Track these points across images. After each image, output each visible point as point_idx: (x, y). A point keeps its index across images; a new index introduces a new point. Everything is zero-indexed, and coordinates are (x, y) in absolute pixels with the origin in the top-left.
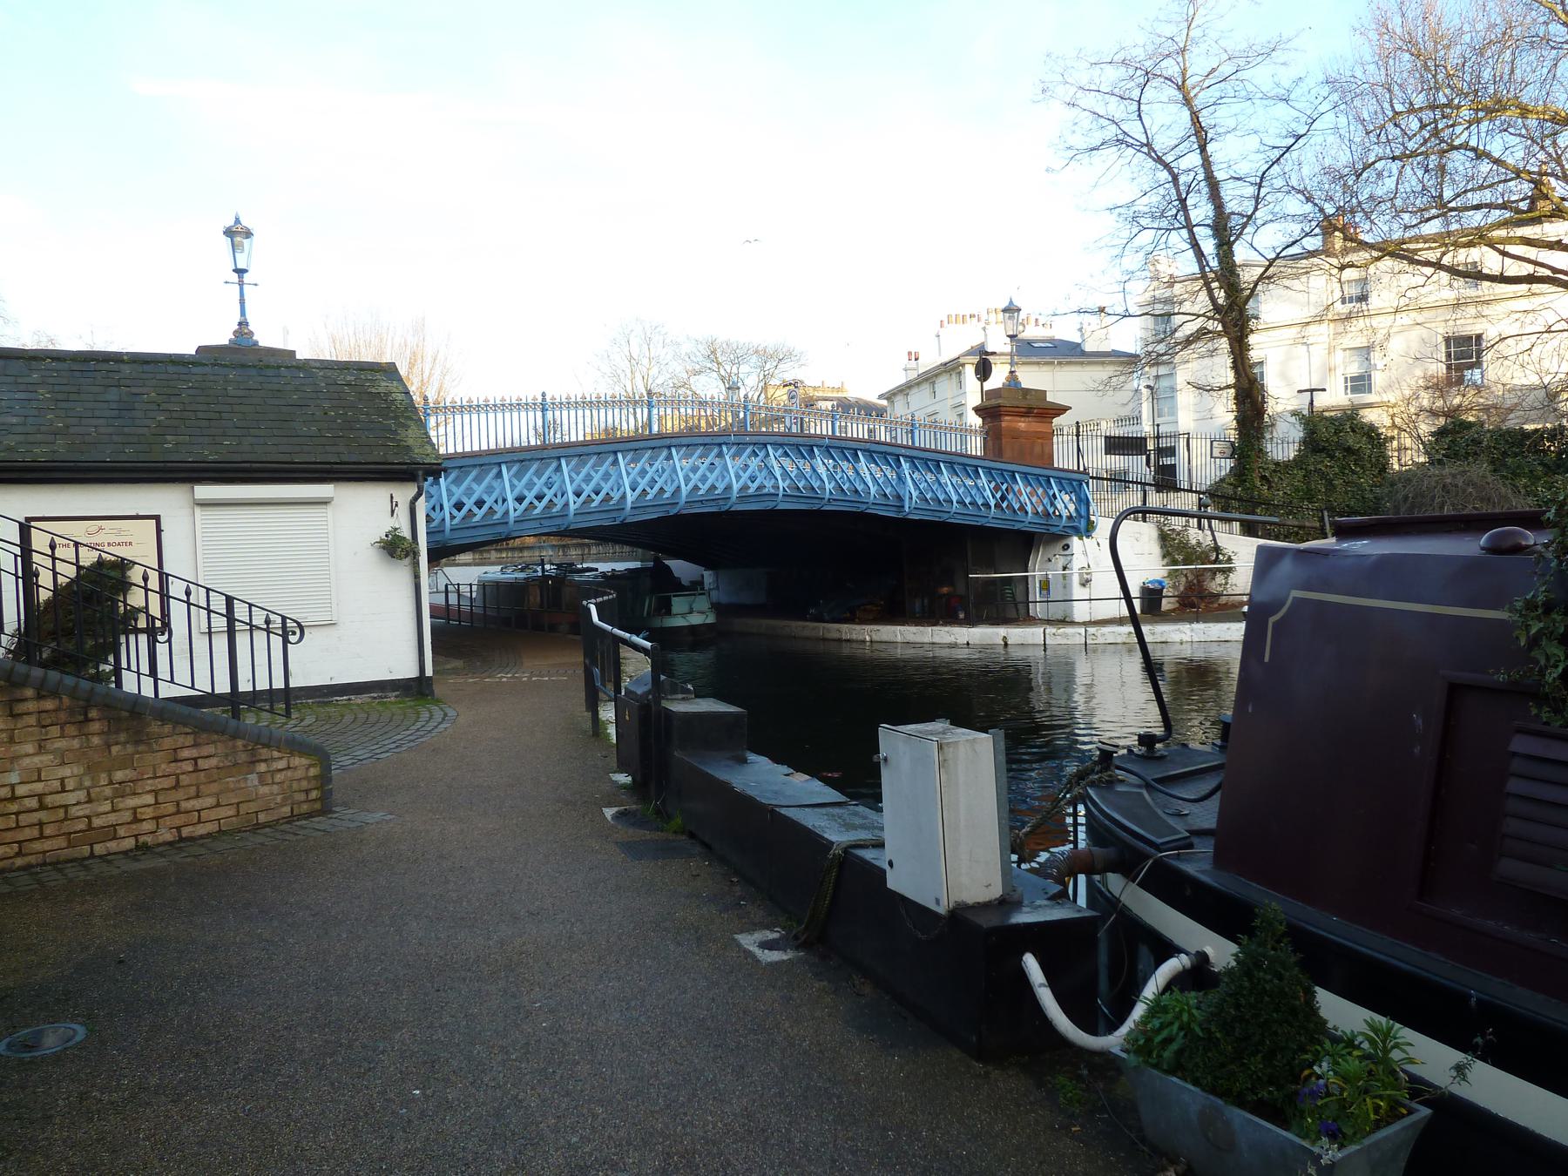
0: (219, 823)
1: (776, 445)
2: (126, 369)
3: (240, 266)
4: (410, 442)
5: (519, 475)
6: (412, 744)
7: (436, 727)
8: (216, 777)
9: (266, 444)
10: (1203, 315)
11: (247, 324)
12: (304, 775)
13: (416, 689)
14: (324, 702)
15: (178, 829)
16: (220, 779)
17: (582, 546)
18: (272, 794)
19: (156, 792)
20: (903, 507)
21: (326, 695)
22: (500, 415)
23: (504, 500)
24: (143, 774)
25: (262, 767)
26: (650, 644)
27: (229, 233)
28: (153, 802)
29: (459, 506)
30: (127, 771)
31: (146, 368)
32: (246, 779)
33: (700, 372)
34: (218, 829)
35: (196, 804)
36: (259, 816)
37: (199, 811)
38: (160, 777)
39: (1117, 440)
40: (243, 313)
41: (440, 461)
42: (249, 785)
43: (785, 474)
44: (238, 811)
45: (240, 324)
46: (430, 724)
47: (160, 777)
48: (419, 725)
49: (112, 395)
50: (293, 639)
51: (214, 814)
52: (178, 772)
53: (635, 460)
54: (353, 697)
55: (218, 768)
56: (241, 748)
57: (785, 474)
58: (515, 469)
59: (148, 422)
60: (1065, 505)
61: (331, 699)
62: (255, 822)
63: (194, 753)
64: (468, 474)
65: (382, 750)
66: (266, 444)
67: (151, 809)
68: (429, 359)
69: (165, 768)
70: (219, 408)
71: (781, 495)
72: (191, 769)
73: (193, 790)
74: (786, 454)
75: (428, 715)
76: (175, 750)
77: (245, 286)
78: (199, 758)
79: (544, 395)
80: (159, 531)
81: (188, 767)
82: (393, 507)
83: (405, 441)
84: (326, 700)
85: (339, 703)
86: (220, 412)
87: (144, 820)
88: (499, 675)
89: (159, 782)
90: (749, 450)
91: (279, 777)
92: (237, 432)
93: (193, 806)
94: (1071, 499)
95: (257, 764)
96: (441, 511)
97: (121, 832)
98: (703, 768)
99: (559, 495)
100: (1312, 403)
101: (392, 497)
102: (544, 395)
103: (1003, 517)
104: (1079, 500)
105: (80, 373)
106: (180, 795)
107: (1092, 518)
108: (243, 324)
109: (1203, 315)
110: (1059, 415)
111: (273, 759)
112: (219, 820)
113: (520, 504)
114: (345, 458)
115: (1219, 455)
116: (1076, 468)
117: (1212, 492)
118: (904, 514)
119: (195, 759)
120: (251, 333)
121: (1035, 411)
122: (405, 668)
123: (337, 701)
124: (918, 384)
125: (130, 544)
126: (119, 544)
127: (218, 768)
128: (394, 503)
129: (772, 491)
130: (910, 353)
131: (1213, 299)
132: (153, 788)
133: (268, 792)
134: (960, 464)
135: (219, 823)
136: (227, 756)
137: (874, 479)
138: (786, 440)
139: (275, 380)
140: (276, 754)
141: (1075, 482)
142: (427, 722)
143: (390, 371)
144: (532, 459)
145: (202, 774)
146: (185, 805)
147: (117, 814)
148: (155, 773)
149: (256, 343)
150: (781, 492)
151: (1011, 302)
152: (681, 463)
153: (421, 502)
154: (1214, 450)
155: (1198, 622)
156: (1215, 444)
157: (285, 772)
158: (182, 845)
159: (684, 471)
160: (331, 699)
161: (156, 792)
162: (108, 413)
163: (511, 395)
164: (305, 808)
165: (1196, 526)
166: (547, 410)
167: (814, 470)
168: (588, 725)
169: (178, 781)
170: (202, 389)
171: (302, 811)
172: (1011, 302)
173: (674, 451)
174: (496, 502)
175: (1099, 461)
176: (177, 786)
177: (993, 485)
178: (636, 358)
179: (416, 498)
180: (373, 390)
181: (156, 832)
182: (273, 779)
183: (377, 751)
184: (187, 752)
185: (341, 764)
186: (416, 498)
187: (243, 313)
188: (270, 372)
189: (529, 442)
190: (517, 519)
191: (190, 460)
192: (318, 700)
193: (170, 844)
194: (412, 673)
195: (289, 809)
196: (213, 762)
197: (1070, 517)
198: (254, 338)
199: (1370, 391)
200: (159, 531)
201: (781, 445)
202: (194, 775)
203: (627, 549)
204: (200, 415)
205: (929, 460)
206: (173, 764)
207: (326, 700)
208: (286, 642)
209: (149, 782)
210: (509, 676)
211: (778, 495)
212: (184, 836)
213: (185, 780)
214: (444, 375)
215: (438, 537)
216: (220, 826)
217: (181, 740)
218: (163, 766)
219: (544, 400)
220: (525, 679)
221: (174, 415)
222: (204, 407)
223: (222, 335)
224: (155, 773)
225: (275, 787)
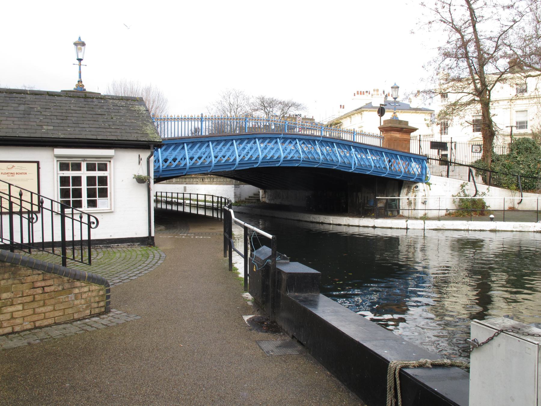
0: (55, 319)
1: (300, 140)
2: (29, 97)
3: (80, 57)
4: (148, 132)
5: (192, 148)
6: (146, 272)
7: (157, 262)
8: (53, 296)
9: (86, 131)
10: (472, 93)
11: (81, 82)
12: (96, 295)
13: (147, 241)
14: (107, 246)
15: (34, 322)
16: (56, 297)
17: (210, 178)
18: (81, 304)
19: (23, 304)
20: (351, 167)
21: (108, 243)
22: (190, 123)
23: (185, 159)
24: (17, 295)
25: (76, 291)
26: (272, 236)
27: (76, 44)
28: (21, 309)
29: (166, 161)
30: (8, 294)
31: (37, 97)
32: (68, 297)
33: (257, 110)
34: (54, 322)
35: (43, 309)
36: (75, 315)
37: (44, 313)
38: (25, 296)
39: (439, 144)
40: (80, 77)
41: (161, 141)
42: (70, 300)
43: (303, 152)
44: (64, 313)
45: (79, 82)
46: (154, 261)
47: (25, 296)
48: (149, 260)
49: (22, 107)
50: (93, 226)
51: (52, 315)
52: (34, 293)
53: (240, 143)
54: (120, 245)
55: (54, 292)
56: (66, 281)
57: (303, 152)
58: (190, 146)
59: (36, 120)
60: (415, 168)
61: (110, 245)
62: (72, 318)
63: (43, 284)
64: (171, 146)
65: (133, 275)
66: (86, 131)
67: (20, 312)
69: (27, 292)
70: (67, 115)
71: (301, 160)
72: (41, 292)
73: (42, 303)
74: (304, 143)
75: (152, 256)
76: (33, 282)
77: (81, 66)
78: (45, 286)
79: (202, 115)
80: (38, 168)
81: (40, 291)
82: (140, 160)
83: (146, 131)
84: (108, 245)
85: (114, 247)
86: (67, 117)
87: (17, 318)
88: (181, 235)
89: (25, 299)
90: (288, 141)
91: (84, 296)
92: (74, 125)
93: (42, 310)
94: (419, 167)
95: (74, 289)
96: (158, 162)
97: (5, 324)
98: (306, 307)
99: (208, 157)
100: (512, 131)
101: (139, 156)
102: (202, 115)
103: (392, 173)
104: (422, 168)
105: (9, 98)
106: (35, 305)
107: (428, 175)
108: (80, 81)
109: (472, 93)
110: (413, 132)
111: (82, 287)
112: (54, 317)
113: (192, 160)
114: (120, 138)
115: (475, 151)
116: (418, 154)
118: (352, 170)
119: (43, 287)
120: (83, 86)
121: (404, 130)
122: (144, 233)
123: (113, 246)
125: (26, 173)
126: (21, 174)
127: (54, 292)
128: (140, 159)
129: (298, 159)
131: (475, 86)
132: (22, 302)
133: (79, 303)
134: (374, 150)
135: (55, 319)
136: (59, 285)
137: (340, 156)
138: (304, 137)
139: (91, 103)
140: (83, 284)
141: (422, 159)
142: (153, 259)
143: (140, 101)
144: (197, 141)
145: (47, 294)
146: (38, 310)
147: (3, 315)
148: (23, 294)
149: (85, 90)
150: (302, 160)
151: (395, 84)
152: (259, 145)
153: (152, 159)
154: (473, 149)
155: (471, 221)
156: (474, 147)
157: (87, 293)
158: (36, 331)
159: (261, 148)
160: (110, 245)
161: (23, 304)
162: (19, 116)
163: (189, 114)
164: (97, 311)
165: (468, 180)
166: (203, 121)
167: (315, 150)
168: (227, 264)
169: (34, 298)
170: (60, 106)
171: (96, 312)
172: (395, 84)
173: (257, 140)
174: (181, 159)
175: (427, 150)
176: (34, 301)
177: (388, 159)
178: (232, 104)
179: (150, 157)
180: (133, 109)
181: (22, 324)
182: (81, 297)
183: (131, 275)
184: (39, 283)
185: (114, 282)
186: (150, 157)
187: (80, 77)
188: (90, 100)
189: (188, 135)
190: (190, 167)
191: (53, 137)
192: (104, 245)
193: (30, 330)
194: (146, 235)
195: (89, 311)
196: (52, 288)
197: (419, 175)
198: (84, 88)
199: (526, 128)
200: (38, 168)
201: (302, 139)
202: (43, 295)
203: (228, 180)
204: (59, 117)
205: (362, 148)
206: (32, 290)
207: (108, 245)
208: (90, 227)
209: (20, 299)
210: (185, 235)
211: (300, 160)
212: (37, 326)
213: (38, 297)
214: (157, 108)
215: (158, 174)
216: (55, 321)
217: (36, 277)
218: (27, 291)
219: (202, 117)
220: (192, 237)
222: (60, 114)
223: (71, 86)
224: (23, 294)
225: (83, 300)
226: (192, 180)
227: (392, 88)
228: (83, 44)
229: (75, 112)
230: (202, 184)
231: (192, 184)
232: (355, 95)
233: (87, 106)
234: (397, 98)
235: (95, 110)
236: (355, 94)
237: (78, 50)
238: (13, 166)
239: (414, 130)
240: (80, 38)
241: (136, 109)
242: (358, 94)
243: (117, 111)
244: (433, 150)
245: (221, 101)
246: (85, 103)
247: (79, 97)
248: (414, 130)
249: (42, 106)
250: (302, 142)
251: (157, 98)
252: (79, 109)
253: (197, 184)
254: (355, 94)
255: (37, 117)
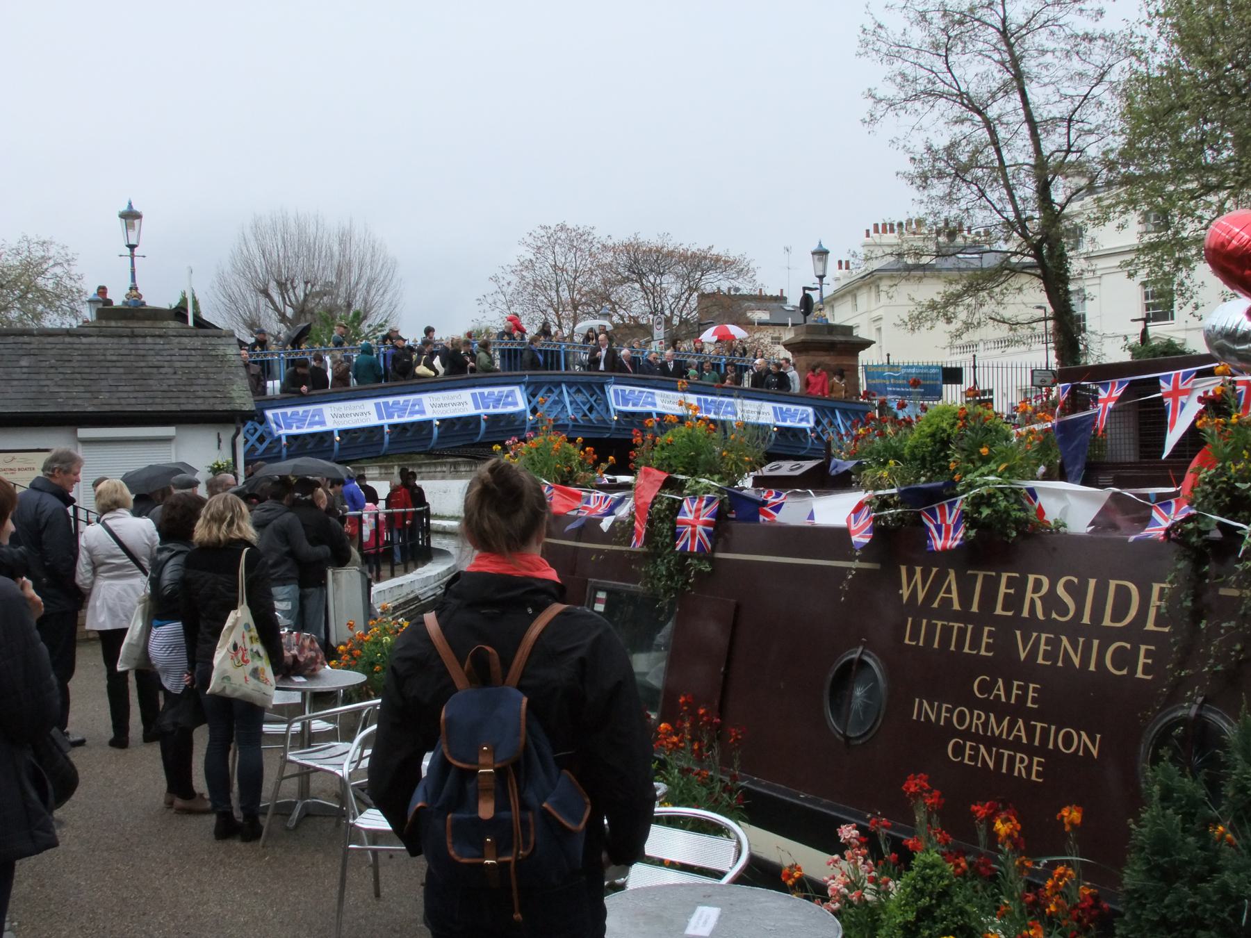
3: (132, 242)
4: (234, 394)
45: (131, 289)
68: (380, 266)
108: (134, 288)
117: (247, 492)
120: (140, 296)
124: (843, 296)
130: (840, 262)
149: (143, 304)
151: (820, 245)
172: (820, 245)
180: (214, 353)
188: (140, 340)
221: (67, 376)
226: (433, 469)
227: (814, 253)
228: (138, 216)
229: (114, 364)
230: (453, 478)
231: (434, 478)
232: (868, 235)
233: (133, 352)
234: (824, 276)
235: (150, 358)
236: (868, 231)
237: (129, 227)
238: (14, 458)
239: (866, 344)
240: (130, 204)
241: (219, 353)
242: (876, 231)
243: (184, 358)
244: (954, 386)
245: (531, 261)
246: (131, 346)
247: (121, 336)
248: (866, 344)
249: (58, 358)
250: (574, 389)
251: (369, 256)
252: (120, 358)
253: (443, 478)
254: (868, 231)
255: (50, 376)
